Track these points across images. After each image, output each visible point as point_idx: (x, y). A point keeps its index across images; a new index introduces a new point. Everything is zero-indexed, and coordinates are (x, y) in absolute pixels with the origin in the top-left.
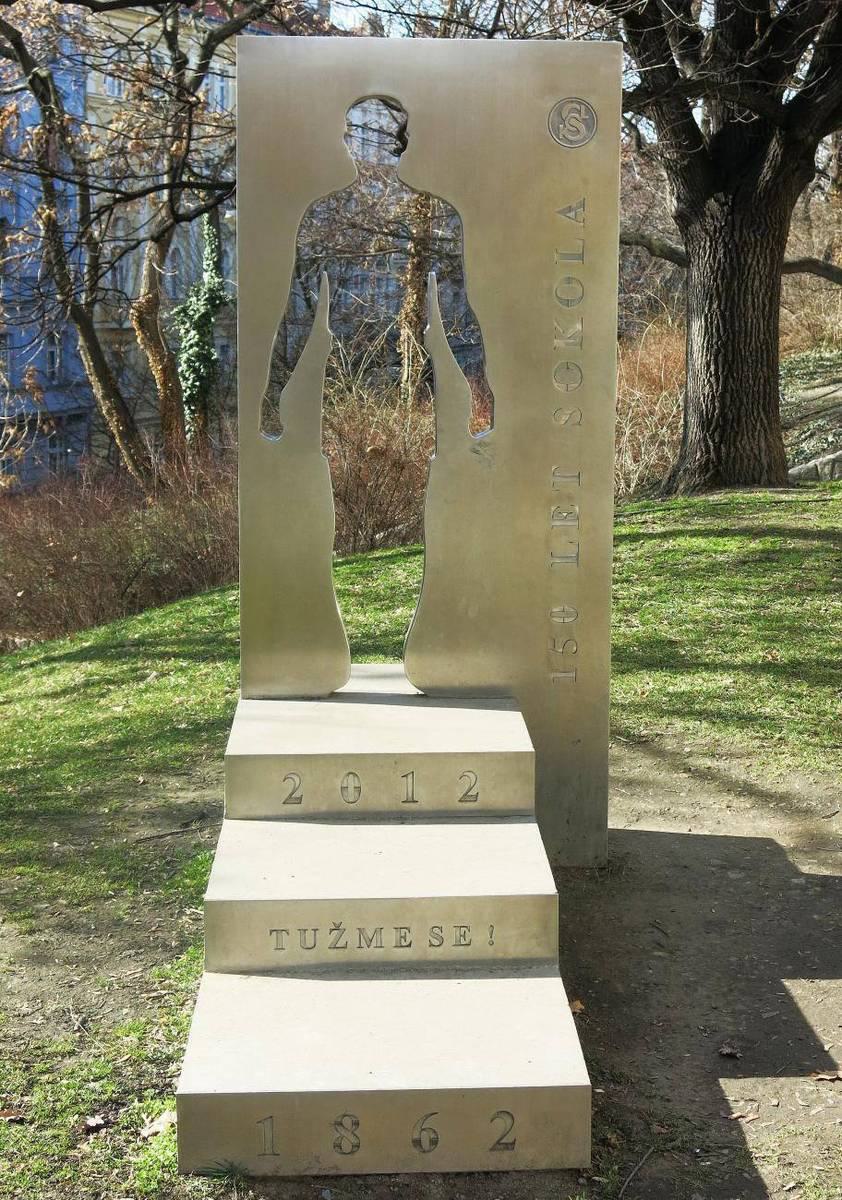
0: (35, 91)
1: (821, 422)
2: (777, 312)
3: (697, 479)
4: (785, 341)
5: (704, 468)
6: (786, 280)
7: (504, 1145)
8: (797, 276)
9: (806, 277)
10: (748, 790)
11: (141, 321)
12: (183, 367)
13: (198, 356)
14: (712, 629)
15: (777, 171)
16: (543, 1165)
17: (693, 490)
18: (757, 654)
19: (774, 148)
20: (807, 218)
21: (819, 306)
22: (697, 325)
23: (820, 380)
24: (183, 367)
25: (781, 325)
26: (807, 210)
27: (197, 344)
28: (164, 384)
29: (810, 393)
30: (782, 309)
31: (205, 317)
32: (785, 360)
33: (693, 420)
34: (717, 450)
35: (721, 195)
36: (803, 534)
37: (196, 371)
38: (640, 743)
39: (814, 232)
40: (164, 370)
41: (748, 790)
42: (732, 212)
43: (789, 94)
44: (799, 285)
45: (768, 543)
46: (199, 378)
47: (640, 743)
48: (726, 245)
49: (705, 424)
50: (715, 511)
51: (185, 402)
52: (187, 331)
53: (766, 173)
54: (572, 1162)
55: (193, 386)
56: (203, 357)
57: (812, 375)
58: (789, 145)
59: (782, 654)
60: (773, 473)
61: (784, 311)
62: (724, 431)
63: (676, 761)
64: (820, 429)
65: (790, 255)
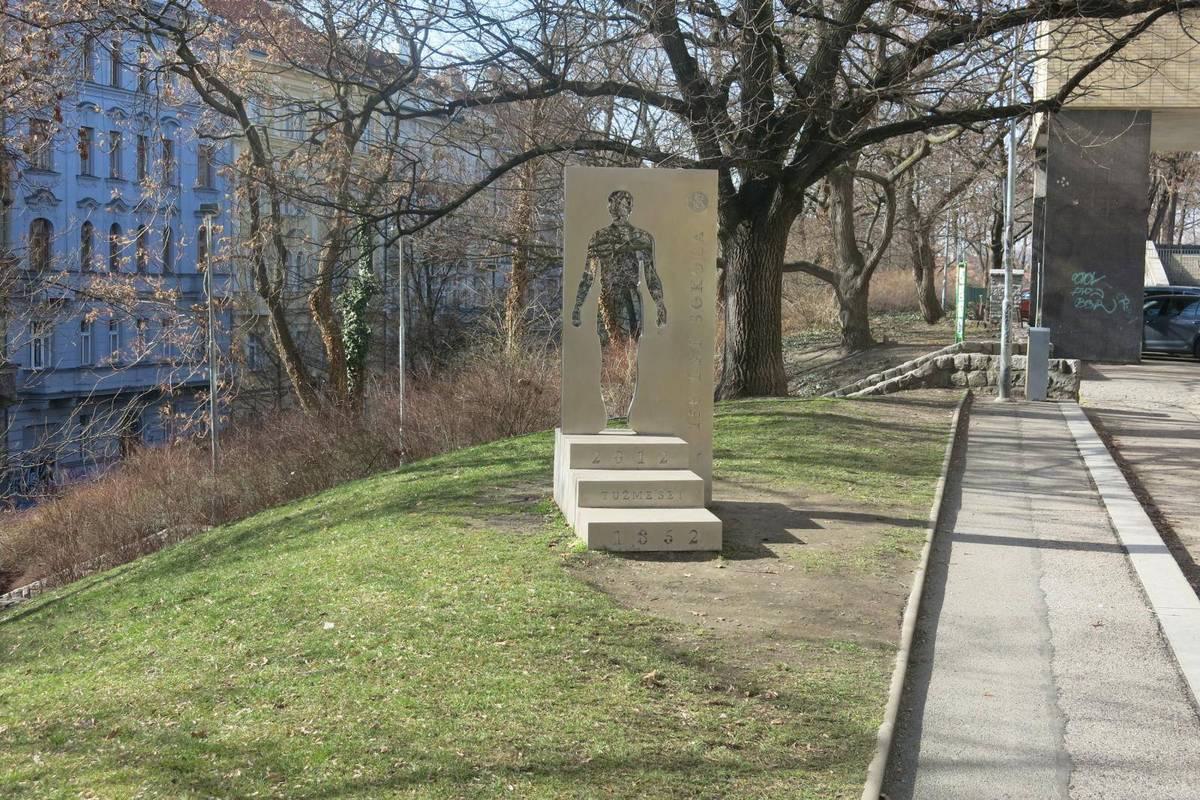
0: (249, 138)
1: (811, 376)
2: (780, 301)
3: (732, 392)
4: (786, 323)
5: (737, 384)
6: (786, 277)
7: (693, 542)
8: (794, 275)
9: (802, 275)
10: (769, 491)
11: (316, 304)
12: (346, 338)
13: (357, 330)
14: (748, 447)
15: (779, 207)
16: (706, 549)
17: (731, 397)
18: (772, 454)
19: (777, 194)
20: (802, 233)
21: (811, 298)
22: (732, 300)
23: (810, 348)
24: (346, 338)
25: (783, 311)
26: (801, 227)
27: (356, 322)
28: (333, 350)
29: (804, 357)
30: (783, 300)
31: (362, 302)
32: (785, 337)
33: (730, 357)
34: (745, 374)
35: (746, 222)
36: (797, 415)
37: (355, 341)
38: (719, 479)
39: (807, 242)
40: (333, 340)
41: (769, 491)
42: (752, 232)
43: (786, 163)
44: (795, 281)
45: (776, 418)
46: (357, 346)
47: (719, 479)
48: (749, 251)
49: (737, 358)
50: (744, 406)
51: (349, 364)
52: (348, 312)
53: (773, 209)
54: (716, 548)
55: (353, 352)
56: (361, 332)
57: (805, 345)
58: (786, 194)
59: (783, 455)
60: (778, 388)
61: (784, 301)
62: (748, 363)
63: (736, 484)
64: (811, 380)
65: (789, 259)
